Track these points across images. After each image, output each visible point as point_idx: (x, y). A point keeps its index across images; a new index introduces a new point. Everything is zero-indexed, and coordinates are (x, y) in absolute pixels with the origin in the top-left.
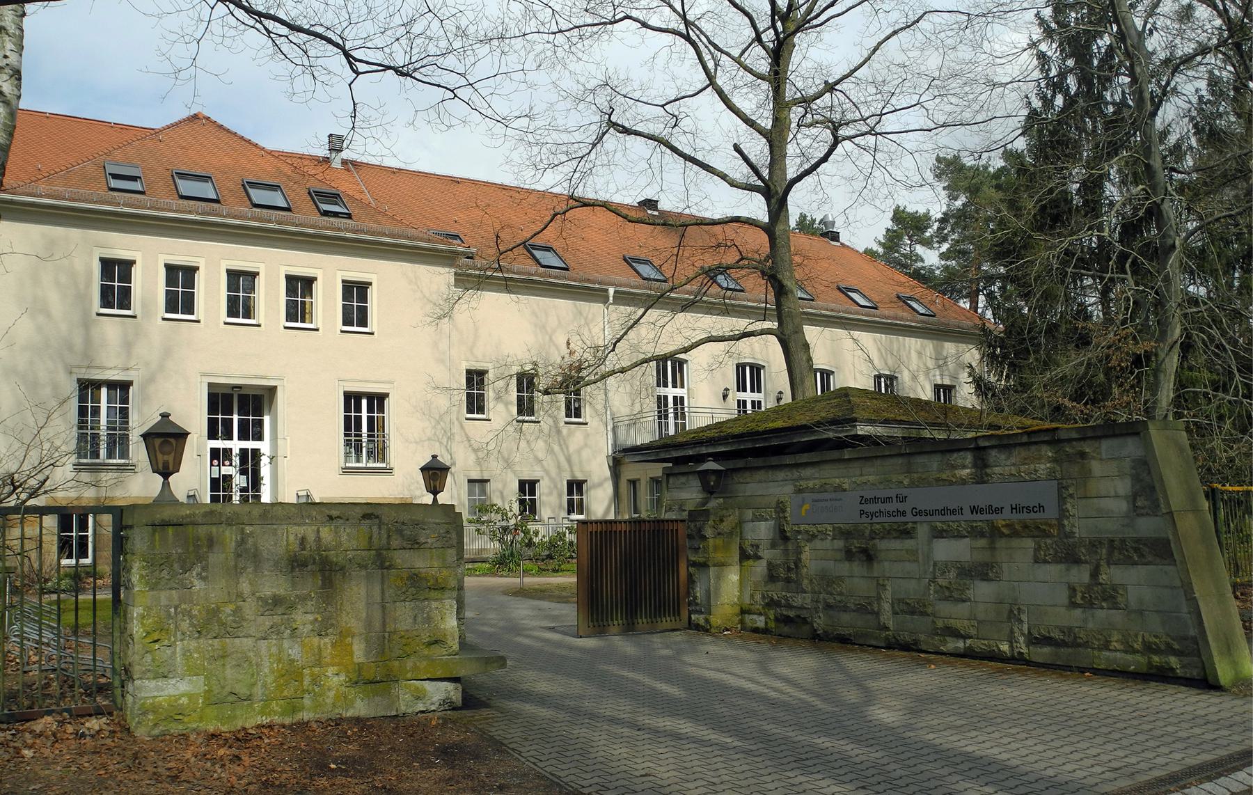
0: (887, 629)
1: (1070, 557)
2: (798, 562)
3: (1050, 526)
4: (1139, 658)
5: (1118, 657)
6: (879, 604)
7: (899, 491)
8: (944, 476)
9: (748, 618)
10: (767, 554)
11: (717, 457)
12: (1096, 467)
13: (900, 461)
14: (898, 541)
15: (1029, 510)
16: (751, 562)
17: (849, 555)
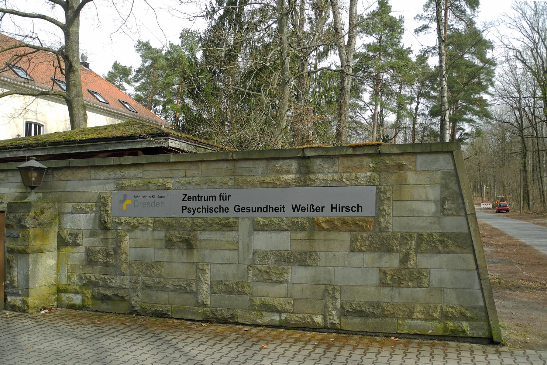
0: (205, 306)
1: (385, 248)
2: (117, 250)
3: (367, 222)
4: (436, 324)
5: (418, 324)
6: (197, 285)
7: (222, 191)
8: (269, 180)
9: (64, 296)
10: (85, 241)
11: (38, 158)
12: (411, 177)
13: (225, 165)
14: (219, 233)
15: (348, 209)
16: (69, 249)
17: (169, 243)
